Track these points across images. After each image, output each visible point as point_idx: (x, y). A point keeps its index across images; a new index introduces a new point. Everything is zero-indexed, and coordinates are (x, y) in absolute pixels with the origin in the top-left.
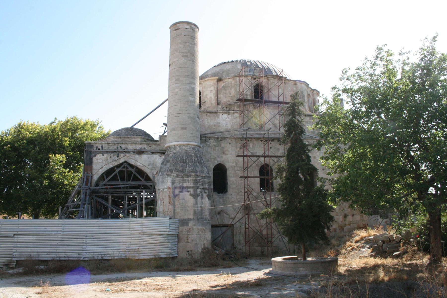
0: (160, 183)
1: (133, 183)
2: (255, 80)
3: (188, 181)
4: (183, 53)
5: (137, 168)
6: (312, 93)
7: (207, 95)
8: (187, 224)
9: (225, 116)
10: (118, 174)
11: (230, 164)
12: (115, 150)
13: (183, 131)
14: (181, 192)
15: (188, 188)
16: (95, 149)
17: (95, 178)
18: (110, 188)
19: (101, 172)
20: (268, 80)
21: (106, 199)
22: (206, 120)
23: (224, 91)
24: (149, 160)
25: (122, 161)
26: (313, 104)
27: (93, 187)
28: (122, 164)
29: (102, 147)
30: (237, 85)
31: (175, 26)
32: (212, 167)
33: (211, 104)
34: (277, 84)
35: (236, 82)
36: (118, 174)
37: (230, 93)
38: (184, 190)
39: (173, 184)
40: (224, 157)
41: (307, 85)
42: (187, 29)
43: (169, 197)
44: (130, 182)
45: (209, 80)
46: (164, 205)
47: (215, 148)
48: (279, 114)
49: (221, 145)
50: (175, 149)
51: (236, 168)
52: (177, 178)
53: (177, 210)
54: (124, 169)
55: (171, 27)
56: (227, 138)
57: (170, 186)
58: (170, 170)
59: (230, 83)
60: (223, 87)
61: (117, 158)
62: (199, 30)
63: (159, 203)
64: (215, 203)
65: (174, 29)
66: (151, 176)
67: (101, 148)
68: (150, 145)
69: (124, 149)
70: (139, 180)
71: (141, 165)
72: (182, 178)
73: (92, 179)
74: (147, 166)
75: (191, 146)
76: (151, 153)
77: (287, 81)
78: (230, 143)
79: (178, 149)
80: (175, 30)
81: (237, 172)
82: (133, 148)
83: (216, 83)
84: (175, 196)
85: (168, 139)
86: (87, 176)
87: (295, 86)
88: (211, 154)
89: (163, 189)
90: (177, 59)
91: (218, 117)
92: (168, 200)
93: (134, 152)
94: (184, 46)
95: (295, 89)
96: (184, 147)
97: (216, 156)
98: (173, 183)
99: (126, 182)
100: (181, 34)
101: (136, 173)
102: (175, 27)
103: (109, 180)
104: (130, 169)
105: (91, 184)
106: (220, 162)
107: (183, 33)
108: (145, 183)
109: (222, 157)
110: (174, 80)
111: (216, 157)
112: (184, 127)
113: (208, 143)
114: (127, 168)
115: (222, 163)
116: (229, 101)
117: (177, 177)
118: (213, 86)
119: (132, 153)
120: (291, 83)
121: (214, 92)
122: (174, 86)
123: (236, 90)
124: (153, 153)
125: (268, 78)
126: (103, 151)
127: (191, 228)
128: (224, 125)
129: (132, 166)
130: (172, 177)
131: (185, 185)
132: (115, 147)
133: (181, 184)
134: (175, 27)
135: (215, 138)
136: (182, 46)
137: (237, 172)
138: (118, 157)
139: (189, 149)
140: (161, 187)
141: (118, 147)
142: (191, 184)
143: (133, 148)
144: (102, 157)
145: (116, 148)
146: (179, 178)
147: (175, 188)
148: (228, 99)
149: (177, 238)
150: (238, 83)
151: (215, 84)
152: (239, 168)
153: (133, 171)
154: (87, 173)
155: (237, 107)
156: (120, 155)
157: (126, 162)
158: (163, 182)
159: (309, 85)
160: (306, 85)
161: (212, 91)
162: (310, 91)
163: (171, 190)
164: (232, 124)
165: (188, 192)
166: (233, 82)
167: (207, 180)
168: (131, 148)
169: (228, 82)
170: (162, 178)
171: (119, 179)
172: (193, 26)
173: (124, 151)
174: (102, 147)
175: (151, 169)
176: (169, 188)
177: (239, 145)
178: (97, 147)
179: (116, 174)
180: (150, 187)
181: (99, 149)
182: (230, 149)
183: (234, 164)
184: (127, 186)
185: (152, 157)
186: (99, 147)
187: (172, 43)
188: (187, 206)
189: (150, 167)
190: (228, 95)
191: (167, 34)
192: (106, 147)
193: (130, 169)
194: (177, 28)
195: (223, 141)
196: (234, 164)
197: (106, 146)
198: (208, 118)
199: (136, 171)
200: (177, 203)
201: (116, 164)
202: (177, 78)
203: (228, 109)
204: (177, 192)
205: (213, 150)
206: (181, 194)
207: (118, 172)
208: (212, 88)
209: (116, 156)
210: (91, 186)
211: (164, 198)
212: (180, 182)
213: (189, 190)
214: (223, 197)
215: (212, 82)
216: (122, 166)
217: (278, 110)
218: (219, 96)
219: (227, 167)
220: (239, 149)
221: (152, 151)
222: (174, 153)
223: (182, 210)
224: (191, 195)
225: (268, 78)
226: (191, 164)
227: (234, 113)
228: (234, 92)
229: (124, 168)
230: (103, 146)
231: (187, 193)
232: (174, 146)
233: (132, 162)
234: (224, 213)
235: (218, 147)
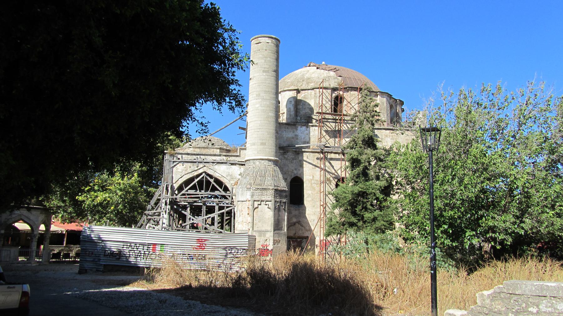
4: (265, 68)
6: (395, 103)
8: (265, 236)
10: (197, 184)
12: (195, 161)
13: (262, 147)
18: (189, 198)
22: (285, 132)
26: (395, 115)
30: (316, 97)
34: (357, 97)
36: (197, 184)
42: (268, 43)
44: (209, 192)
47: (292, 161)
49: (298, 158)
51: (313, 182)
63: (238, 214)
69: (204, 160)
81: (313, 185)
86: (167, 185)
88: (288, 166)
90: (258, 74)
91: (297, 130)
94: (265, 61)
97: (293, 168)
99: (205, 192)
101: (214, 184)
106: (296, 175)
108: (223, 193)
110: (255, 95)
111: (293, 170)
113: (286, 156)
115: (299, 176)
123: (315, 101)
124: (232, 164)
128: (303, 138)
130: (251, 190)
135: (293, 151)
137: (313, 185)
138: (197, 167)
150: (318, 95)
152: (315, 181)
153: (212, 181)
158: (242, 194)
159: (391, 96)
160: (388, 96)
162: (393, 101)
163: (251, 203)
167: (284, 194)
180: (228, 197)
183: (311, 178)
190: (308, 106)
196: (311, 178)
198: (287, 130)
199: (214, 181)
202: (257, 93)
213: (267, 203)
226: (269, 178)
235: (296, 160)
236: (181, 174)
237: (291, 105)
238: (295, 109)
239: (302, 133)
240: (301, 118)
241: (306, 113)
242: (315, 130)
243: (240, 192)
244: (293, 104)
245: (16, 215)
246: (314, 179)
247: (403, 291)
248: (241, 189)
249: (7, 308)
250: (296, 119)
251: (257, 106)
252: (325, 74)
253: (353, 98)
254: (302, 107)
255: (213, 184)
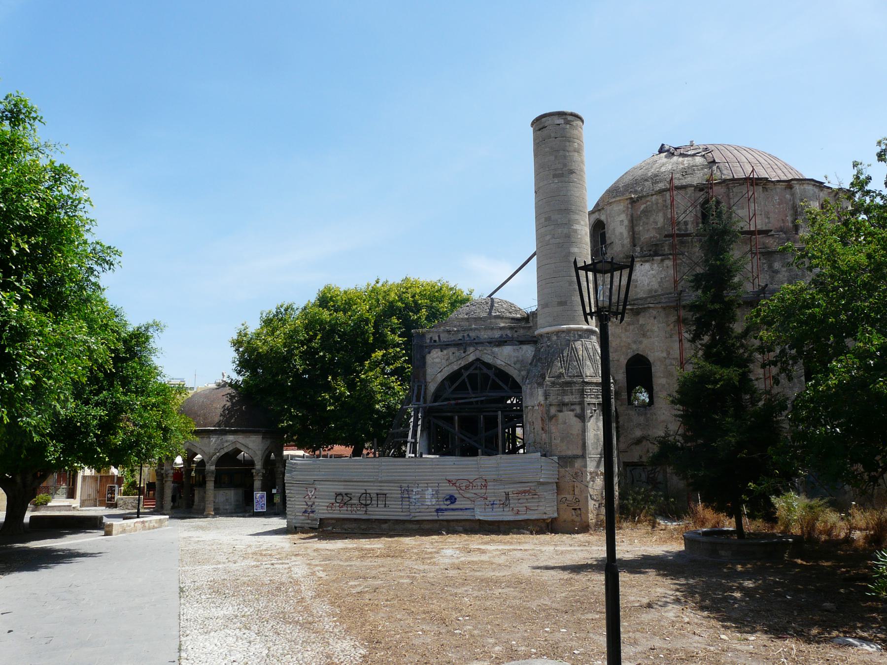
0: (528, 396)
1: (490, 394)
2: (702, 193)
3: (572, 393)
4: (556, 170)
5: (497, 368)
7: (614, 229)
8: (572, 466)
9: (647, 266)
11: (657, 354)
12: (460, 342)
14: (561, 411)
15: (572, 404)
16: (428, 341)
17: (432, 388)
19: (440, 378)
20: (728, 188)
21: (450, 420)
23: (645, 220)
24: (516, 354)
25: (471, 358)
27: (429, 404)
28: (471, 364)
29: (439, 336)
31: (538, 123)
32: (624, 361)
33: (623, 246)
35: (665, 201)
37: (656, 223)
38: (564, 408)
39: (546, 399)
40: (645, 341)
41: (819, 185)
42: (559, 124)
43: (542, 420)
45: (617, 201)
46: (534, 432)
48: (752, 253)
49: (638, 321)
50: (549, 339)
52: (552, 389)
53: (555, 441)
54: (477, 372)
55: (532, 124)
56: (649, 307)
57: (542, 402)
58: (541, 374)
59: (654, 202)
60: (644, 212)
61: (463, 355)
62: (583, 121)
64: (183, 655)
65: (537, 129)
66: (518, 380)
67: (437, 339)
68: (516, 329)
70: (500, 388)
71: (503, 363)
72: (560, 388)
73: (427, 391)
74: (513, 365)
75: (576, 333)
76: (517, 343)
77: (770, 186)
78: (655, 318)
79: (554, 338)
80: (540, 130)
81: (669, 367)
82: (488, 335)
83: (630, 206)
84: (551, 418)
85: (540, 321)
87: (788, 191)
88: (621, 338)
89: (533, 407)
90: (546, 182)
92: (541, 425)
93: (490, 343)
94: (556, 157)
95: (788, 196)
96: (563, 335)
97: (629, 340)
98: (546, 396)
100: (550, 137)
101: (494, 378)
102: (540, 123)
103: (455, 390)
104: (485, 370)
105: (425, 398)
106: (637, 352)
107: (553, 135)
109: (641, 342)
110: (543, 220)
111: (629, 344)
112: (563, 300)
114: (480, 369)
116: (654, 237)
117: (553, 387)
118: (624, 211)
119: (488, 344)
120: (780, 186)
121: (626, 223)
122: (543, 230)
123: (665, 215)
125: (727, 185)
126: (441, 344)
127: (579, 471)
128: (646, 284)
129: (488, 366)
131: (567, 399)
132: (460, 336)
133: (560, 398)
134: (540, 123)
136: (552, 158)
138: (464, 352)
139: (572, 338)
140: (529, 404)
141: (464, 336)
142: (576, 398)
143: (488, 335)
144: (440, 353)
145: (461, 338)
146: (556, 389)
147: (550, 405)
148: (653, 233)
149: (555, 487)
151: (628, 208)
153: (490, 373)
154: (419, 381)
155: (669, 249)
156: (468, 349)
157: (478, 360)
158: (532, 394)
160: (814, 185)
161: (622, 221)
164: (659, 280)
165: (573, 410)
166: (660, 201)
168: (486, 336)
169: (652, 202)
170: (530, 389)
171: (469, 388)
172: (570, 118)
173: (475, 341)
174: (439, 336)
175: (520, 371)
176: (540, 405)
177: (673, 318)
178: (431, 338)
179: (464, 381)
181: (435, 341)
182: (655, 328)
183: (664, 355)
184: (483, 399)
185: (520, 350)
186: (434, 339)
187: (536, 155)
188: (571, 434)
189: (518, 366)
191: (529, 133)
192: (445, 337)
193: (485, 370)
194: (541, 126)
195: (642, 314)
196: (664, 355)
197: (446, 335)
200: (553, 429)
201: (463, 363)
203: (653, 252)
204: (553, 410)
205: (624, 331)
206: (560, 414)
207: (467, 376)
208: (623, 217)
209: (462, 352)
210: (425, 402)
211: (534, 420)
212: (558, 395)
213: (573, 407)
214: (646, 414)
215: (622, 204)
216: (473, 368)
217: (749, 246)
218: (636, 229)
219: (651, 359)
220: (672, 326)
221: (520, 339)
222: (548, 346)
223: (562, 440)
224: (576, 416)
225: (727, 185)
227: (662, 260)
228: (662, 220)
229: (476, 369)
230: (441, 335)
231: (569, 412)
232: (548, 333)
233: (488, 359)
234: (648, 442)
236: (439, 366)
237: (624, 228)
238: (631, 233)
239: (643, 276)
240: (641, 249)
241: (651, 238)
242: (668, 267)
243: (528, 391)
244: (626, 226)
245: (229, 443)
246: (670, 357)
247: (174, 661)
248: (529, 386)
249: (494, 537)
250: (634, 251)
251: (548, 238)
252: (685, 162)
253: (737, 199)
254: (644, 228)
255: (493, 380)
